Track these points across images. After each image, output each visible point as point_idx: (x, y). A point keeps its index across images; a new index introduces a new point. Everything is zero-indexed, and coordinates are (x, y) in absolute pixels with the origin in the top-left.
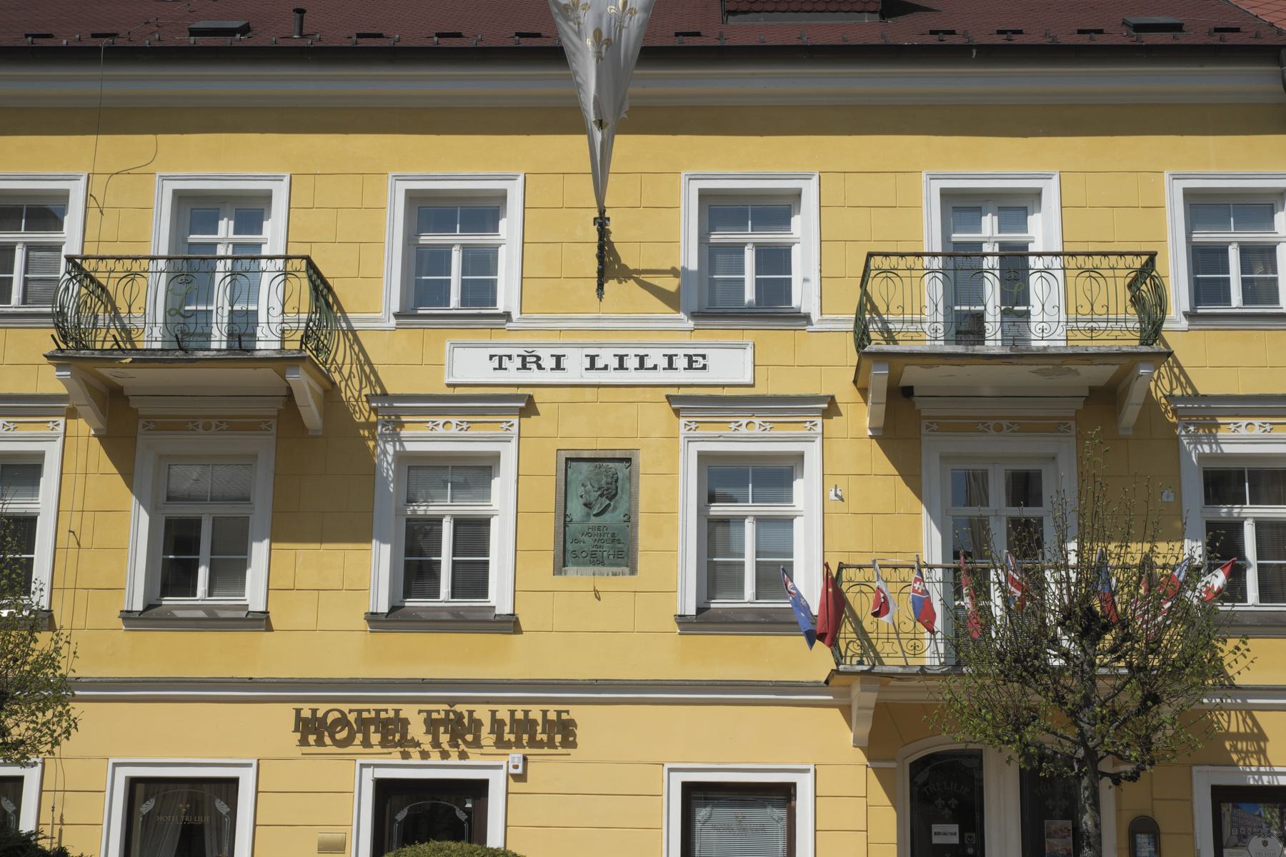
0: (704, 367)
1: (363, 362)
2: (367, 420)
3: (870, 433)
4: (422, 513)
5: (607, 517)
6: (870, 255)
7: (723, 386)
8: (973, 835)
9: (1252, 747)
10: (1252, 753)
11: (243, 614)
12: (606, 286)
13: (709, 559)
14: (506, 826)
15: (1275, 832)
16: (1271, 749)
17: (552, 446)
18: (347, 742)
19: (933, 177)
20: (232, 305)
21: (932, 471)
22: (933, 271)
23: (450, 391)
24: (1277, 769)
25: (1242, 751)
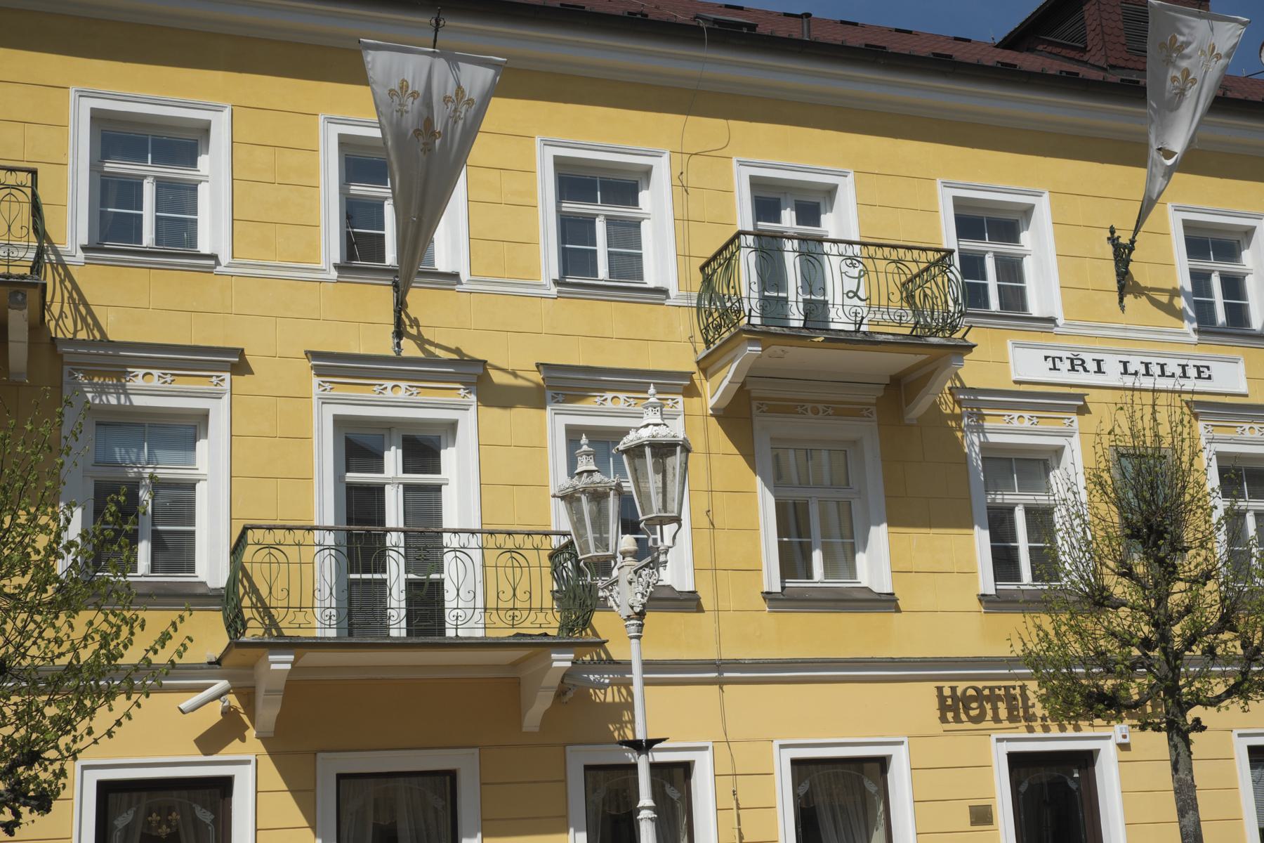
0: (1209, 378)
1: (77, 302)
2: (953, 411)
3: (711, 412)
4: (1000, 501)
12: (1125, 300)
13: (154, 528)
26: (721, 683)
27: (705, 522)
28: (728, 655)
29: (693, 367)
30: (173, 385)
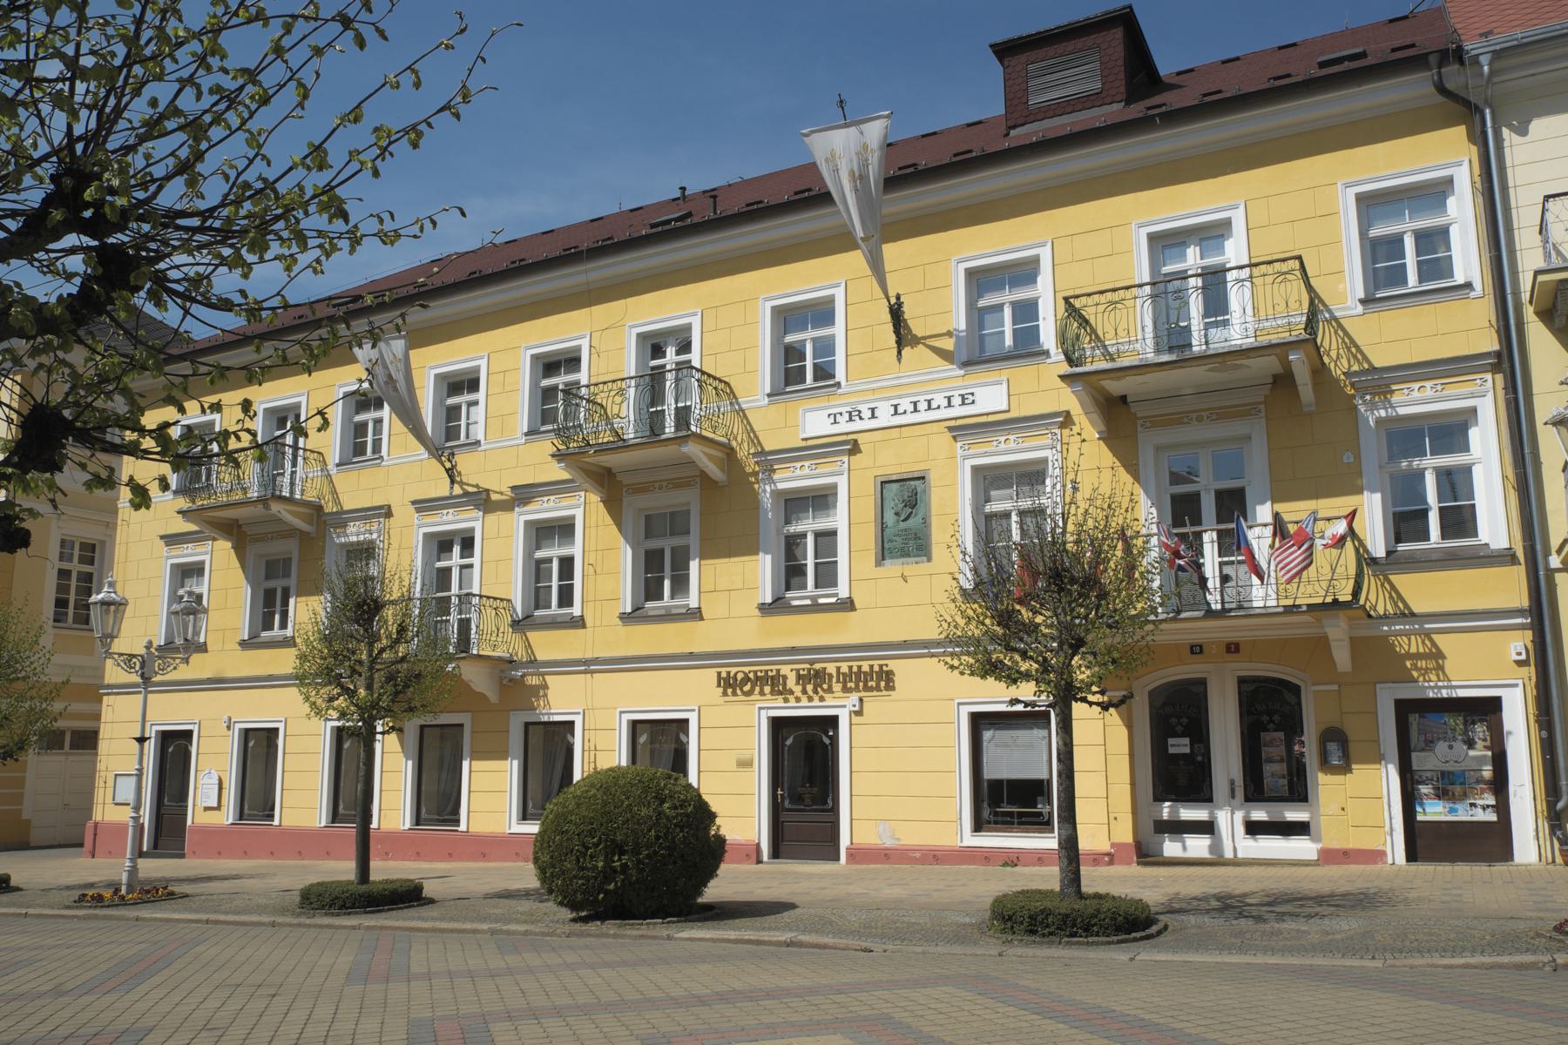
0: (973, 402)
3: (1097, 436)
5: (911, 522)
6: (1299, 258)
7: (987, 414)
8: (1201, 745)
9: (1432, 664)
10: (1431, 669)
11: (684, 611)
14: (851, 748)
15: (1460, 738)
16: (1449, 666)
17: (871, 474)
18: (750, 693)
19: (1347, 186)
20: (676, 402)
22: (1243, 280)
23: (804, 444)
24: (1454, 683)
25: (1422, 669)
30: (1444, 392)
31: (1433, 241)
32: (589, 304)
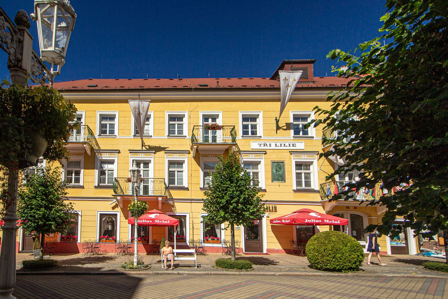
5: (280, 172)
6: (194, 126)
21: (202, 163)
26: (191, 202)
27: (190, 176)
28: (193, 198)
29: (190, 149)
31: (180, 126)
32: (273, 102)
